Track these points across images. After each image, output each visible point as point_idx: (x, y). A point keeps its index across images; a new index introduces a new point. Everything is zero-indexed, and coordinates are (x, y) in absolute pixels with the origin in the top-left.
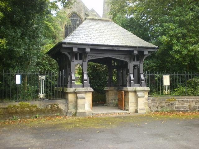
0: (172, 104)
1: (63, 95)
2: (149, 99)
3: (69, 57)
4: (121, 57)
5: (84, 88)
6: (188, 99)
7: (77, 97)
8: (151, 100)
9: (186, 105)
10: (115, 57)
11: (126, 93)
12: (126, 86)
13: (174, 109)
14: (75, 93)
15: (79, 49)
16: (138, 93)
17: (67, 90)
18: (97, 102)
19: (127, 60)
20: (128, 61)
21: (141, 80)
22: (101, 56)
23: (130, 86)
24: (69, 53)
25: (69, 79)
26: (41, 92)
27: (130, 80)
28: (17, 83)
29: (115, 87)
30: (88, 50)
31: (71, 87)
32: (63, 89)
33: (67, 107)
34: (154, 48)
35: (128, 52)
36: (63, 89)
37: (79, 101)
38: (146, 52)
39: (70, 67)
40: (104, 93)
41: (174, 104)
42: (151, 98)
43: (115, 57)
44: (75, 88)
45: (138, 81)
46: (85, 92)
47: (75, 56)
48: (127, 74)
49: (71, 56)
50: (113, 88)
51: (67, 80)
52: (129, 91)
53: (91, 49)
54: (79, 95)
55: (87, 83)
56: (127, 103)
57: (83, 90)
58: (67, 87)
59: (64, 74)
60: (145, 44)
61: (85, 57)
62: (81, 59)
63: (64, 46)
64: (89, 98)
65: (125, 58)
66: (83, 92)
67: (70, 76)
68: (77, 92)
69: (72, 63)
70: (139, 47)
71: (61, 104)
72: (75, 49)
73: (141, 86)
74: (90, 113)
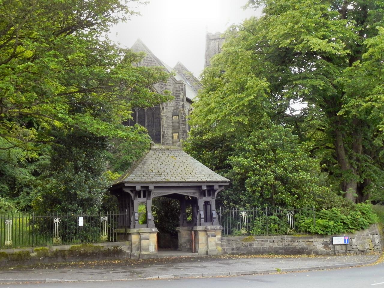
0: (250, 245)
1: (126, 236)
2: (222, 239)
3: (132, 195)
4: (189, 193)
5: (148, 228)
6: (268, 238)
7: (140, 237)
8: (225, 241)
9: (267, 245)
10: (183, 193)
11: (196, 232)
12: (178, 226)
13: (253, 250)
14: (139, 233)
15: (142, 187)
16: (208, 233)
17: (130, 231)
18: (82, 93)
19: (197, 195)
20: (197, 197)
21: (213, 218)
22: (166, 193)
23: (200, 225)
24: (132, 191)
25: (132, 219)
26: (245, 218)
27: (201, 218)
28: (80, 225)
29: (189, 227)
30: (151, 187)
31: (134, 228)
32: (126, 231)
33: (130, 249)
34: (225, 182)
35: (197, 187)
36: (126, 231)
37: (143, 242)
38: (216, 187)
39: (133, 206)
40: (175, 235)
41: (253, 244)
42: (225, 238)
43: (183, 193)
44: (205, 226)
45: (208, 219)
46: (149, 232)
47: (138, 194)
48: (197, 212)
49: (134, 194)
50: (186, 228)
51: (130, 221)
52: (199, 230)
53: (155, 187)
54: (143, 236)
55: (151, 223)
56: (197, 245)
57: (147, 230)
58: (129, 227)
59: (126, 214)
60: (217, 177)
61: (149, 195)
62: (144, 196)
63: (126, 185)
64: (153, 238)
65: (194, 193)
66: (147, 232)
67: (133, 216)
68: (141, 233)
69: (135, 202)
70: (207, 182)
71: (124, 246)
72: (138, 188)
73: (213, 224)
74: (154, 255)
